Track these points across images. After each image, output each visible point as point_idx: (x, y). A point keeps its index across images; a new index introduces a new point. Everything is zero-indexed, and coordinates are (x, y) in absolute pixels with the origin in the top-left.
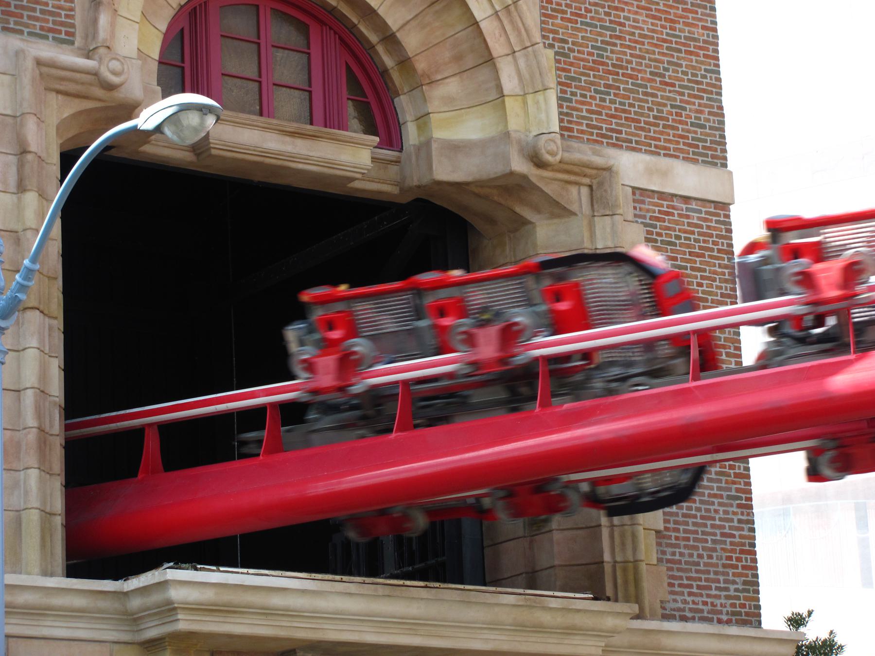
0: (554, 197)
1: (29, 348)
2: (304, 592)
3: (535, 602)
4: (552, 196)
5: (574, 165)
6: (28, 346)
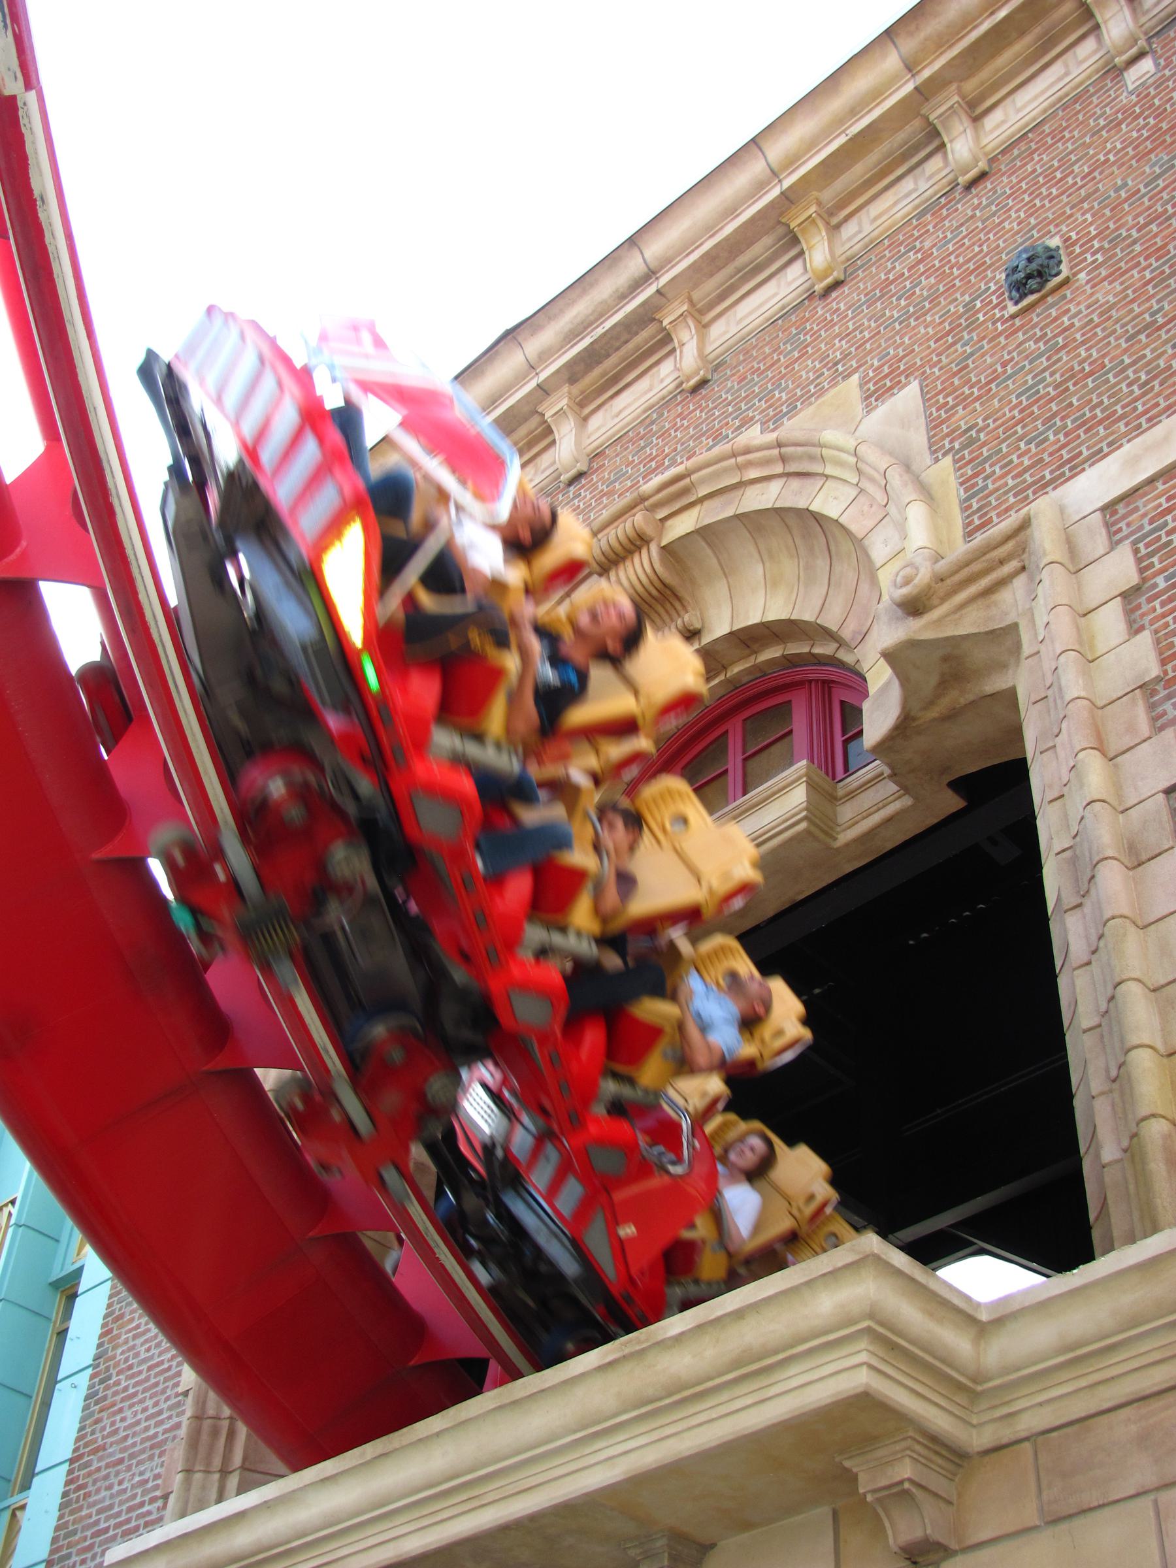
0: (983, 629)
1: (1128, 980)
2: (266, 1506)
3: (639, 1342)
4: (977, 631)
5: (967, 564)
6: (1124, 977)
